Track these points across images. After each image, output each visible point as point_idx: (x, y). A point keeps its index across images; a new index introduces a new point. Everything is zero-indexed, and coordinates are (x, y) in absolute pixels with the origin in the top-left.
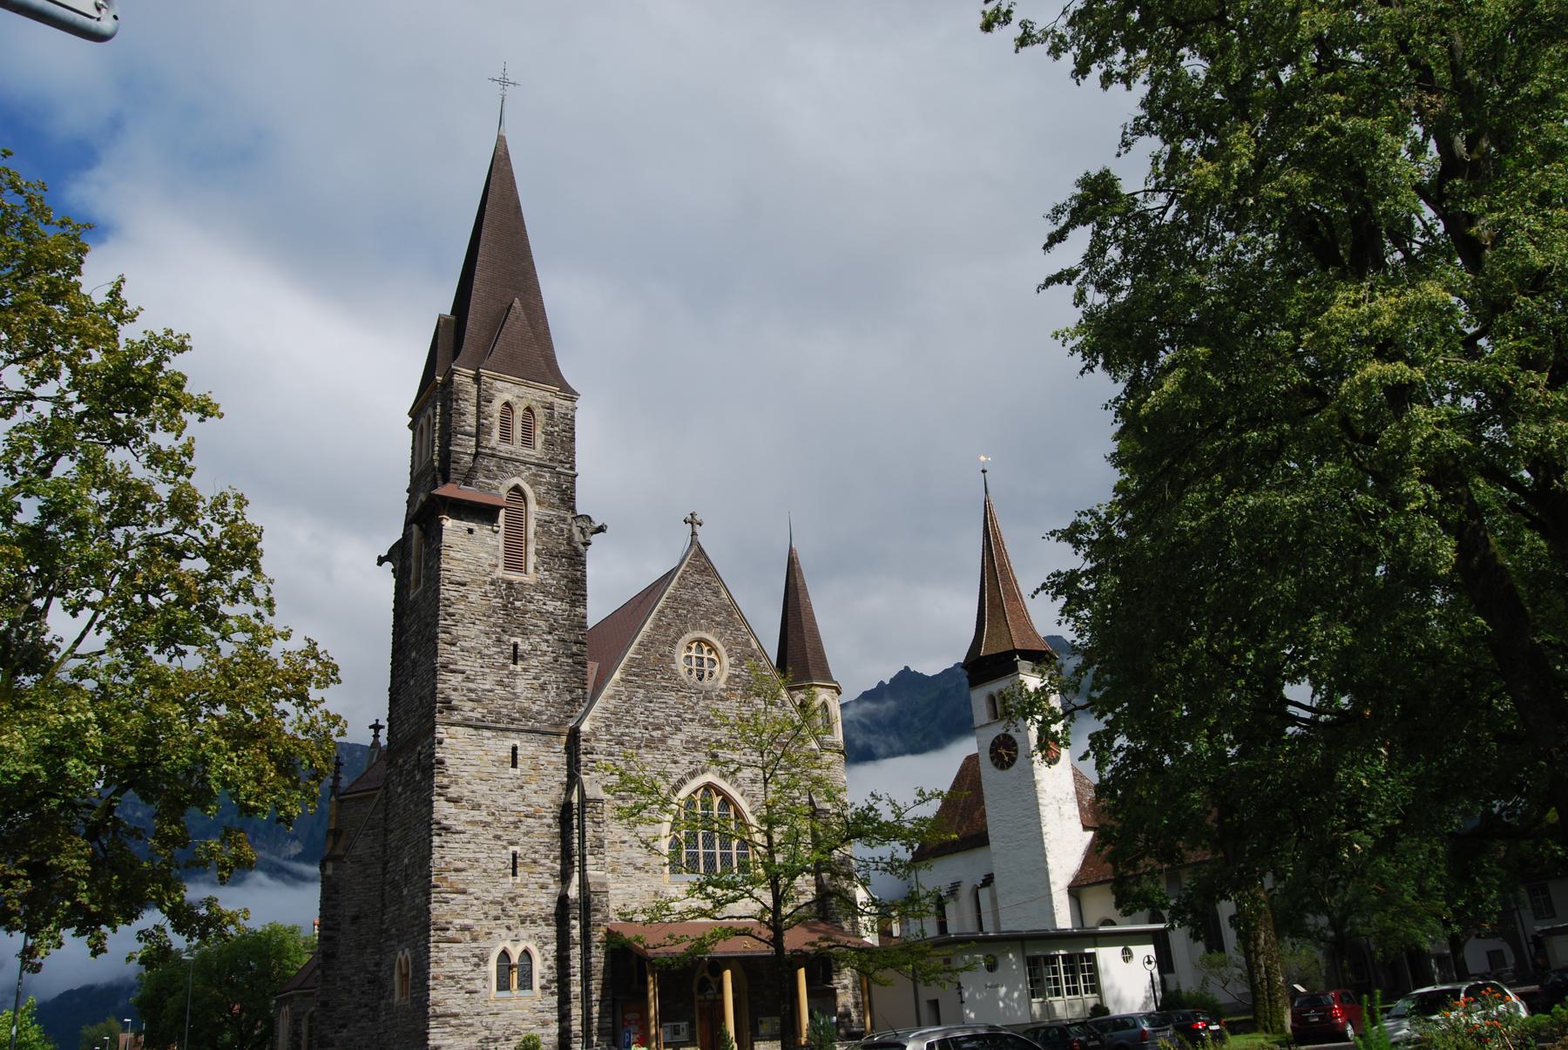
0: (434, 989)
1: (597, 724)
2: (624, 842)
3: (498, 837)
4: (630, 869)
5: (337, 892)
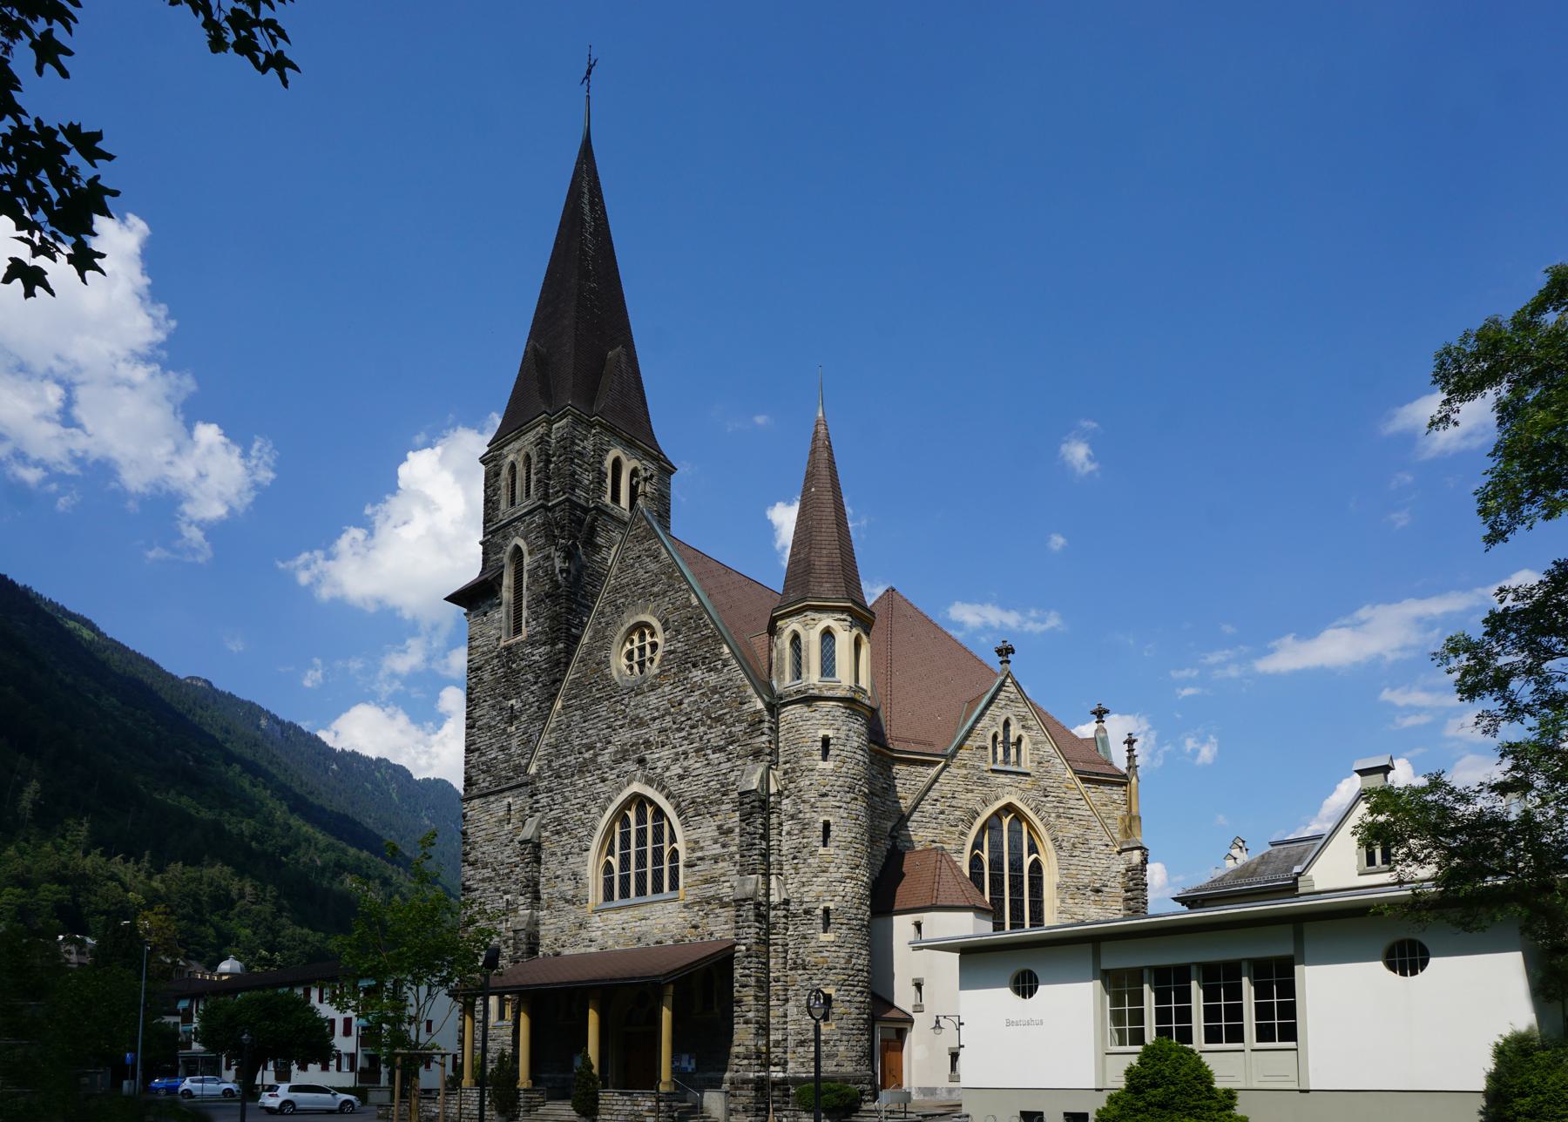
1: (541, 763)
2: (557, 877)
3: (497, 890)
4: (561, 904)
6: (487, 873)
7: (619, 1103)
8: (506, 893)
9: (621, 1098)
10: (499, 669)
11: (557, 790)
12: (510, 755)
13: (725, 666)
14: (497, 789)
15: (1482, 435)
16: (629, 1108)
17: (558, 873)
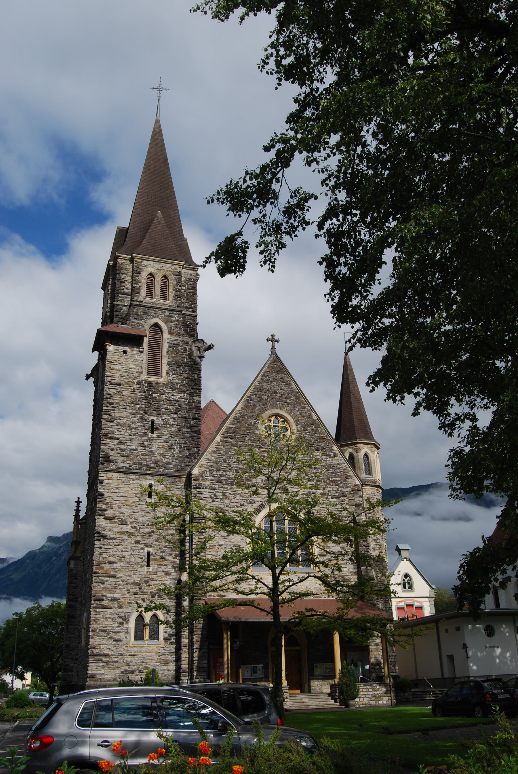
0: (92, 638)
1: (204, 470)
3: (138, 542)
5: (76, 579)
6: (127, 528)
7: (364, 690)
8: (147, 546)
9: (365, 687)
11: (218, 489)
12: (151, 452)
16: (371, 693)
17: (221, 543)
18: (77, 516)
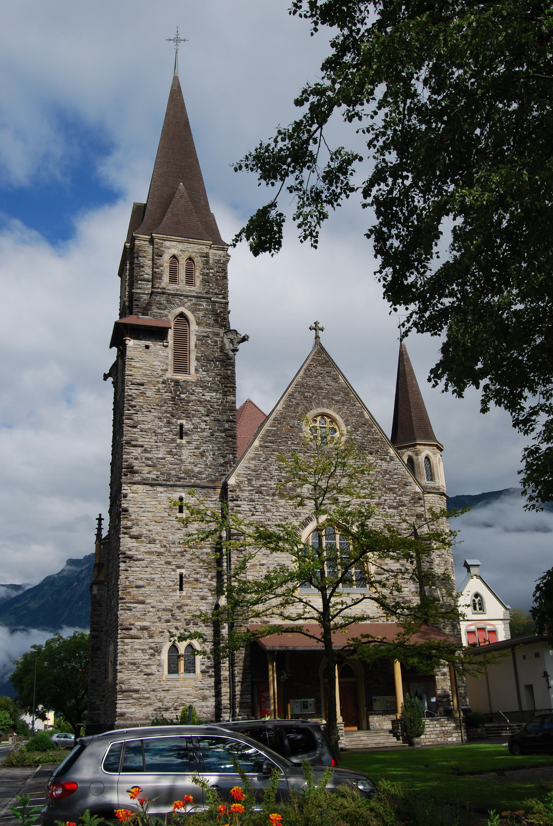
0: (121, 672)
3: (168, 563)
7: (431, 726)
8: (179, 567)
10: (166, 392)
11: (258, 501)
13: (392, 460)
14: (165, 482)
15: (539, 436)
16: (439, 729)
17: (263, 562)
18: (99, 535)
